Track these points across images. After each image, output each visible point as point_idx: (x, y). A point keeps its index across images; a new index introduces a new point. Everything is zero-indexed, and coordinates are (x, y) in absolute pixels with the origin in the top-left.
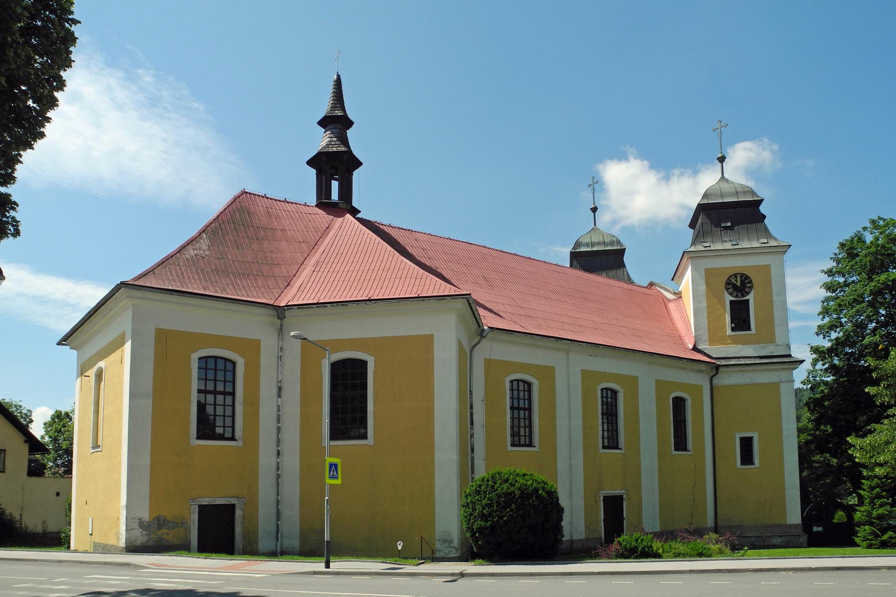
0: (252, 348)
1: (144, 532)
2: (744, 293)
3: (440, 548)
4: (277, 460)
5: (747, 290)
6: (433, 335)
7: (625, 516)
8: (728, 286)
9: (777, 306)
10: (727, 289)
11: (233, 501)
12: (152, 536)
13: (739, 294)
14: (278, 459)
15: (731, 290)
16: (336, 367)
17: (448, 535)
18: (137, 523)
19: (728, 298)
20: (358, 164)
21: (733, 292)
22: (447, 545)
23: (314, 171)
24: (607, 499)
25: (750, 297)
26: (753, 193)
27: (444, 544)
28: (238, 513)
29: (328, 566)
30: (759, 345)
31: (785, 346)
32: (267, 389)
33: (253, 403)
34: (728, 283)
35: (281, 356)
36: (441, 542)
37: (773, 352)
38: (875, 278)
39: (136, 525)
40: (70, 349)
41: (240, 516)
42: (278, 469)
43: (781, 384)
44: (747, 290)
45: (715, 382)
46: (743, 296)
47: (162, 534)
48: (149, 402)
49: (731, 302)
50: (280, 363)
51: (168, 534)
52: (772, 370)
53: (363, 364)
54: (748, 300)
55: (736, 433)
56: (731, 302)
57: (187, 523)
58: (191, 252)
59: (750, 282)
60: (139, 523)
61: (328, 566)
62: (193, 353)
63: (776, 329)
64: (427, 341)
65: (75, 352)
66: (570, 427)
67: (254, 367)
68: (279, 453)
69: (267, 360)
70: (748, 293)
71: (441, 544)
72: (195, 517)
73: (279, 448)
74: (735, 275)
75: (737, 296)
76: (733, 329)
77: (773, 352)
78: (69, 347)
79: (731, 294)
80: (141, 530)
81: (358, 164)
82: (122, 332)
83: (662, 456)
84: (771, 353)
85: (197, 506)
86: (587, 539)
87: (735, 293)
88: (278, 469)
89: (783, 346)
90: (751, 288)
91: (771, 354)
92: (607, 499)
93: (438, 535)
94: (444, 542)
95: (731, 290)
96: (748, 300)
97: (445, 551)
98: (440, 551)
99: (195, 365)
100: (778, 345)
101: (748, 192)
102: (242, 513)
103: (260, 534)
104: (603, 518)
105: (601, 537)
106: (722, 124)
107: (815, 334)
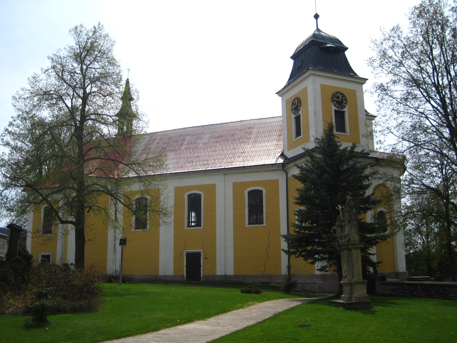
5: (344, 104)
7: (202, 264)
19: (334, 108)
20: (346, 49)
21: (336, 104)
23: (345, 52)
24: (189, 255)
38: (417, 188)
44: (344, 104)
46: (342, 108)
49: (335, 111)
54: (344, 112)
58: (326, 71)
59: (346, 99)
66: (224, 182)
70: (344, 107)
74: (294, 100)
75: (338, 108)
79: (335, 105)
81: (346, 49)
83: (238, 226)
86: (175, 276)
90: (346, 103)
92: (189, 255)
99: (202, 224)
104: (185, 264)
107: (383, 141)
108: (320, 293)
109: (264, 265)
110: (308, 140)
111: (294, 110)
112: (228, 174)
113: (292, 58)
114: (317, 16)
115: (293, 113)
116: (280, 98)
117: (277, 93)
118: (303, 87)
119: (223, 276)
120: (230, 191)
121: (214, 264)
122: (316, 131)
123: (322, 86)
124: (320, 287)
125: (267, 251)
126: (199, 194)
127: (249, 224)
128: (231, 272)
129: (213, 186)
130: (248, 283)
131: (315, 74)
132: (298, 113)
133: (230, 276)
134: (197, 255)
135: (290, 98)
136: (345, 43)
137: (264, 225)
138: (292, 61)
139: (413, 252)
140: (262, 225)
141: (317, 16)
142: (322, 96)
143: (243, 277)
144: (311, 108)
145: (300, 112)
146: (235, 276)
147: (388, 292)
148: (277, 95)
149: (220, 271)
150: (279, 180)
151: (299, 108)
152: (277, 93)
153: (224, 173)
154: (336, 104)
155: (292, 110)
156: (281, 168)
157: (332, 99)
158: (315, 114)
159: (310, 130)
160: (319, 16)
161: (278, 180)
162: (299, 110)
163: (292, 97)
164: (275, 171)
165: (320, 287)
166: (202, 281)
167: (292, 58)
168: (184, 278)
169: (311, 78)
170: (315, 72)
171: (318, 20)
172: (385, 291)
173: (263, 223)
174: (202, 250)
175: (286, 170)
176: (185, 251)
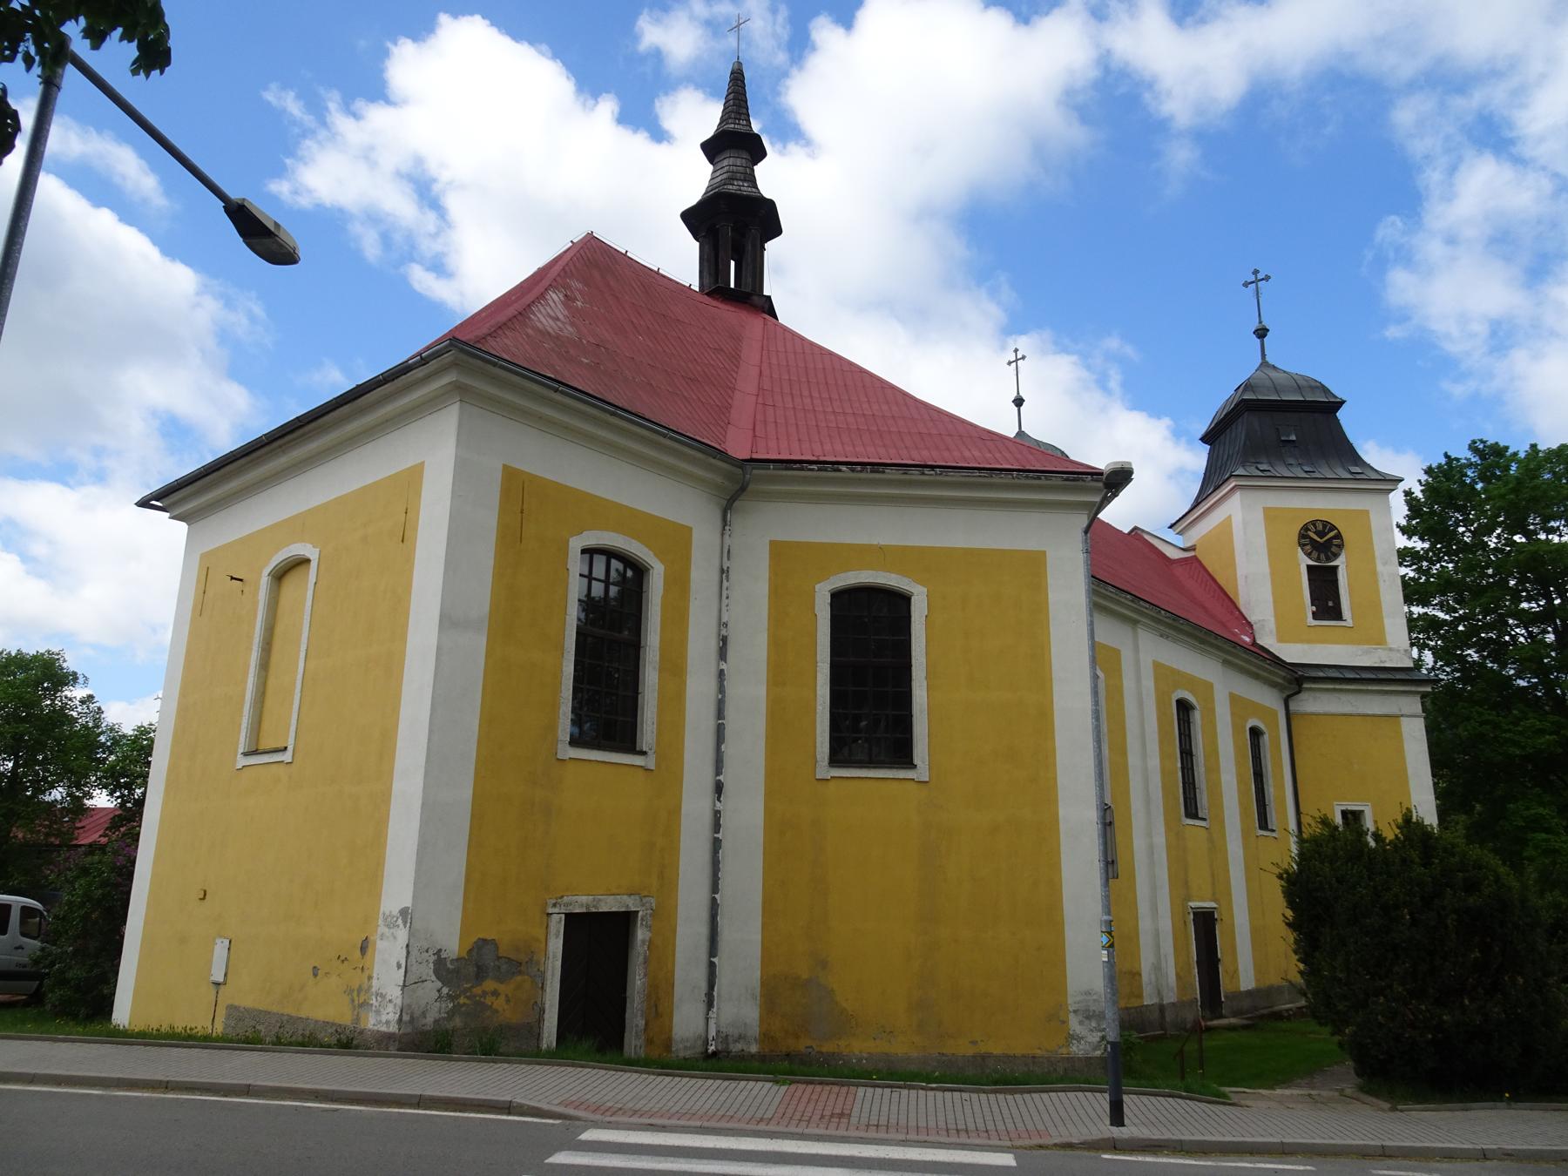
0: (676, 542)
1: (445, 990)
2: (1329, 554)
3: (1078, 1032)
4: (715, 805)
5: (1334, 549)
6: (1044, 553)
8: (1303, 541)
9: (1384, 581)
10: (1302, 546)
11: (631, 904)
12: (462, 1000)
13: (1322, 556)
14: (718, 804)
15: (1308, 547)
16: (844, 601)
17: (1095, 1000)
18: (431, 965)
19: (1304, 561)
21: (1312, 552)
22: (1094, 1024)
25: (1340, 562)
26: (1325, 390)
27: (1087, 1022)
28: (641, 934)
29: (1117, 1117)
30: (1361, 647)
31: (1402, 652)
32: (700, 644)
33: (675, 668)
34: (1303, 535)
35: (728, 568)
36: (1081, 1018)
37: (1385, 661)
39: (428, 971)
40: (170, 518)
41: (643, 942)
42: (717, 826)
43: (1402, 718)
44: (1334, 549)
45: (1293, 707)
46: (1328, 559)
47: (484, 994)
48: (481, 642)
49: (1309, 567)
50: (725, 584)
51: (495, 993)
52: (1387, 692)
53: (901, 601)
54: (1336, 567)
55: (1335, 803)
56: (1309, 567)
57: (538, 963)
60: (435, 963)
61: (1117, 1117)
62: (572, 537)
63: (1387, 621)
64: (1032, 566)
65: (182, 527)
67: (679, 583)
68: (719, 789)
69: (702, 575)
70: (1336, 556)
71: (1081, 1023)
72: (556, 945)
73: (721, 778)
75: (1318, 560)
76: (1316, 616)
77: (1385, 661)
78: (168, 514)
79: (1309, 555)
80: (439, 984)
82: (420, 461)
84: (1381, 662)
85: (563, 916)
87: (1315, 554)
88: (717, 826)
89: (1398, 651)
90: (1341, 546)
91: (1382, 665)
93: (1072, 1001)
94: (1088, 1018)
95: (1308, 547)
96: (1336, 567)
97: (1090, 1039)
98: (1079, 1039)
100: (1391, 649)
101: (1317, 387)
102: (648, 935)
103: (678, 989)
104: (1195, 958)
105: (1196, 999)
106: (1260, 277)
141: (1261, 333)
154: (1312, 552)
171: (1022, 408)
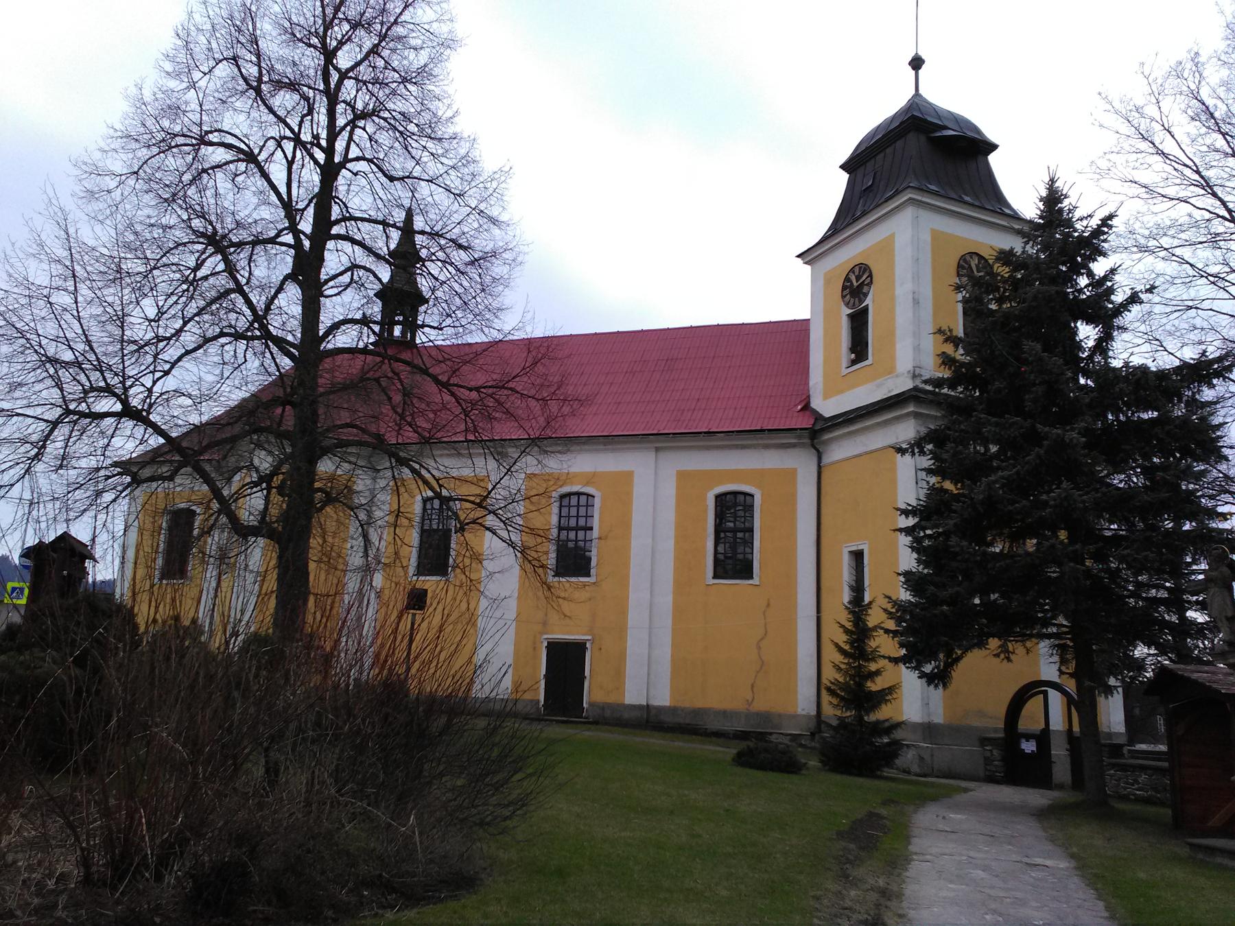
7: (587, 673)
20: (993, 147)
24: (556, 649)
66: (656, 473)
81: (993, 147)
92: (556, 649)
104: (544, 671)
108: (925, 776)
109: (752, 686)
110: (890, 370)
111: (848, 296)
112: (671, 448)
113: (843, 167)
114: (917, 63)
115: (847, 305)
116: (808, 267)
117: (798, 256)
118: (887, 235)
119: (640, 707)
120: (669, 490)
121: (619, 673)
122: (917, 349)
123: (936, 236)
124: (921, 759)
125: (759, 648)
126: (746, 494)
127: (715, 577)
128: (662, 698)
129: (629, 476)
130: (708, 731)
131: (921, 201)
132: (861, 302)
133: (660, 709)
134: (578, 649)
135: (840, 265)
136: (991, 134)
137: (756, 581)
138: (844, 177)
139: (1077, 658)
140: (751, 582)
141: (917, 63)
142: (934, 260)
143: (697, 712)
144: (903, 289)
145: (868, 301)
146: (673, 710)
147: (1138, 792)
148: (799, 259)
149: (633, 695)
150: (799, 470)
151: (865, 289)
152: (798, 256)
153: (658, 445)
155: (843, 297)
156: (807, 441)
157: (958, 273)
158: (916, 302)
159: (898, 346)
160: (923, 62)
161: (795, 470)
162: (866, 295)
163: (847, 262)
164: (788, 447)
165: (921, 759)
166: (586, 718)
167: (843, 167)
168: (538, 709)
169: (909, 213)
170: (923, 196)
171: (920, 72)
172: (1125, 789)
173: (752, 578)
174: (589, 638)
175: (818, 447)
176: (546, 636)
